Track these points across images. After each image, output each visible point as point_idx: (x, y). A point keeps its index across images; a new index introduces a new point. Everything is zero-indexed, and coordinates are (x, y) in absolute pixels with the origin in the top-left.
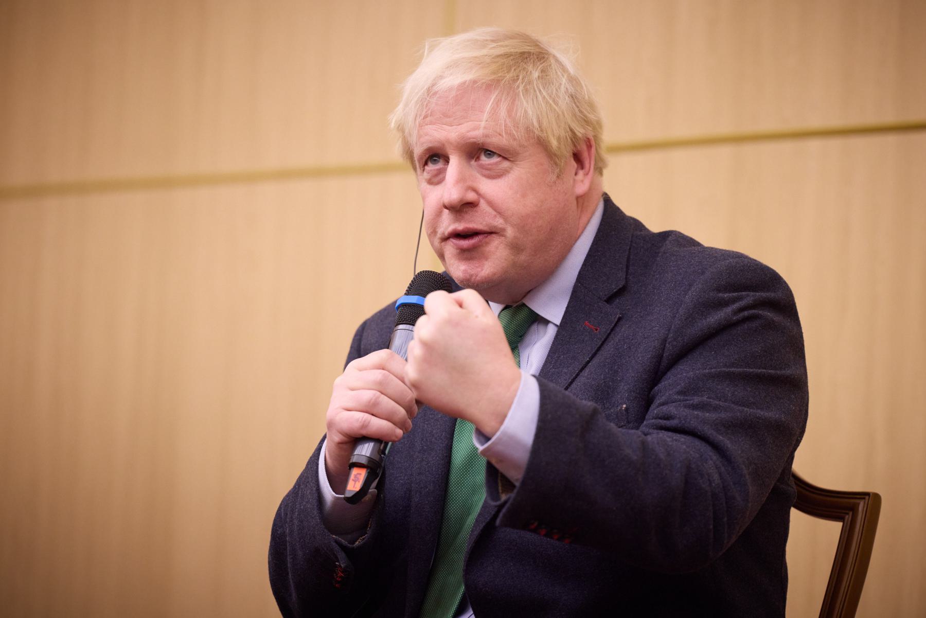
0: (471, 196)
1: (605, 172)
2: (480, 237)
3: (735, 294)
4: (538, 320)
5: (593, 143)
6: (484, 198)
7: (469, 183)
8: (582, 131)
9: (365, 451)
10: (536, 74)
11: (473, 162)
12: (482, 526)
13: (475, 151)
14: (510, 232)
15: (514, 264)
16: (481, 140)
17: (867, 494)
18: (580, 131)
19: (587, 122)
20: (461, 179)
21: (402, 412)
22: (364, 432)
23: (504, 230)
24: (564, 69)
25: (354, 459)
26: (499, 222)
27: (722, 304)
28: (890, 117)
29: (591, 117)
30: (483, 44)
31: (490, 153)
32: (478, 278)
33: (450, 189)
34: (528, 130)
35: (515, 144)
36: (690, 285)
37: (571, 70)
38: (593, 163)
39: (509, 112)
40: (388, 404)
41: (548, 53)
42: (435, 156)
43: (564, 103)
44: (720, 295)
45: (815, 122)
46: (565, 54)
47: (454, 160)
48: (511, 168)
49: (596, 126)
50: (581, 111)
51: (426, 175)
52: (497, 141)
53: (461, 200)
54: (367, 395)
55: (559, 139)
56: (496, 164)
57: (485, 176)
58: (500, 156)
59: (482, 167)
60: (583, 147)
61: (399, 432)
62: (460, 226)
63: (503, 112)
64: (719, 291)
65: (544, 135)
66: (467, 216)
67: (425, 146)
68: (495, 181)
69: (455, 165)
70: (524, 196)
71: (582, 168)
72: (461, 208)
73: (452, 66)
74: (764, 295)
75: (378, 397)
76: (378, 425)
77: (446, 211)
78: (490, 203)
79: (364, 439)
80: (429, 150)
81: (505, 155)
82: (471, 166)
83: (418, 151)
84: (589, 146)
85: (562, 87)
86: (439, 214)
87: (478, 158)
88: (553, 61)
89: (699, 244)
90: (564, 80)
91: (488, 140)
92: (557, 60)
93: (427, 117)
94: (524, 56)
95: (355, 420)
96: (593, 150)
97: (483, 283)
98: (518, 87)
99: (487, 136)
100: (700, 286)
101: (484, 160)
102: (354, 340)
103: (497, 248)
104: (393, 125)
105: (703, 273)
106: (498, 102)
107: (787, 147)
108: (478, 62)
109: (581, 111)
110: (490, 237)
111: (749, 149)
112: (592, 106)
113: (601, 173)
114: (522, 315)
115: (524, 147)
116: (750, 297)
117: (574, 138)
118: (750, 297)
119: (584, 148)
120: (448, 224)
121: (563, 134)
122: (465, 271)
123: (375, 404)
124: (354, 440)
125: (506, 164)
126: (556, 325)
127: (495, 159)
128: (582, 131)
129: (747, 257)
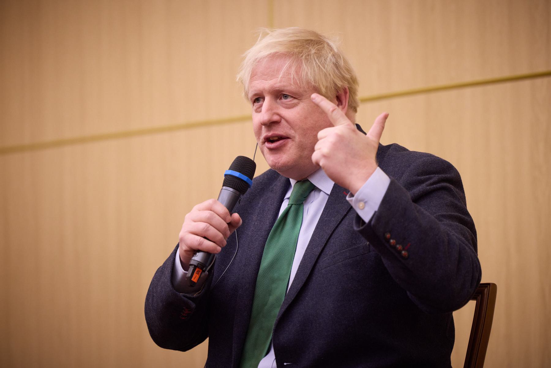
0: (276, 118)
1: (358, 109)
2: (281, 142)
3: (427, 176)
4: (314, 188)
5: (348, 90)
6: (284, 118)
7: (275, 111)
8: (341, 83)
9: (198, 257)
10: (313, 51)
11: (278, 100)
12: (286, 306)
13: (279, 94)
14: (297, 138)
15: (300, 157)
16: (282, 88)
17: (489, 284)
18: (339, 83)
19: (343, 78)
20: (270, 109)
21: (221, 235)
22: (200, 248)
23: (294, 137)
24: (331, 49)
25: (192, 262)
26: (291, 132)
27: (420, 182)
28: (507, 74)
29: (348, 76)
30: (285, 35)
31: (286, 96)
32: (280, 164)
33: (263, 116)
34: (308, 83)
35: (301, 90)
36: (403, 174)
37: (336, 50)
38: (347, 102)
39: (297, 72)
40: (213, 231)
41: (324, 42)
42: (258, 98)
43: (329, 67)
44: (419, 178)
45: (468, 79)
46: (335, 42)
47: (267, 99)
48: (299, 103)
49: (353, 81)
50: (340, 73)
51: (255, 108)
52: (291, 88)
53: (269, 120)
54: (202, 226)
55: (326, 88)
56: (290, 101)
57: (284, 107)
58: (292, 97)
59: (282, 103)
60: (342, 92)
61: (219, 249)
62: (270, 134)
63: (293, 69)
64: (418, 176)
65: (317, 85)
66: (274, 128)
67: (253, 93)
68: (290, 110)
69: (267, 102)
70: (306, 118)
71: (342, 105)
72: (270, 124)
73: (268, 46)
74: (443, 175)
75: (208, 227)
76: (208, 244)
77: (263, 126)
78: (287, 121)
79: (199, 251)
80: (255, 95)
81: (296, 96)
82: (277, 102)
83: (250, 95)
84: (346, 93)
85: (328, 58)
86: (260, 129)
87: (281, 99)
88: (326, 45)
89: (408, 150)
90: (330, 55)
91: (286, 88)
92: (328, 45)
93: (253, 76)
94: (309, 42)
95: (195, 240)
96: (348, 95)
97: (282, 167)
98: (302, 56)
99: (284, 86)
100: (408, 174)
101: (284, 100)
102: (235, 160)
103: (290, 148)
104: (237, 80)
105: (410, 166)
106: (290, 67)
107: (454, 93)
108: (280, 44)
109: (340, 73)
110: (286, 140)
111: (433, 96)
112: (349, 71)
113: (355, 110)
114: (306, 185)
115: (305, 91)
116: (436, 178)
117: (337, 88)
118: (436, 178)
119: (343, 94)
120: (265, 133)
121: (329, 85)
122: (273, 161)
123: (207, 230)
124: (194, 251)
125: (295, 101)
126: (328, 195)
127: (289, 99)
128: (341, 83)
129: (433, 156)
